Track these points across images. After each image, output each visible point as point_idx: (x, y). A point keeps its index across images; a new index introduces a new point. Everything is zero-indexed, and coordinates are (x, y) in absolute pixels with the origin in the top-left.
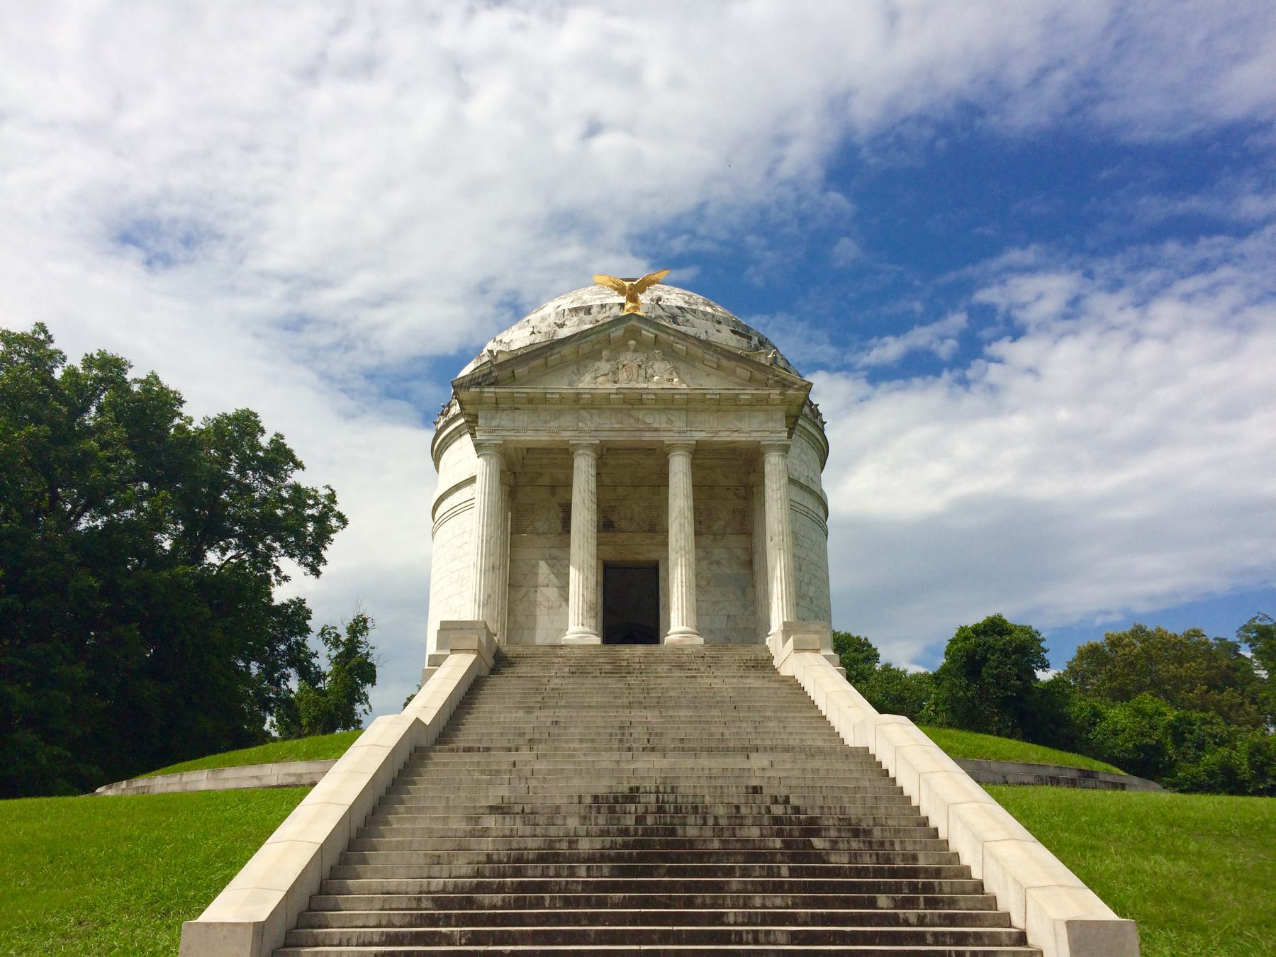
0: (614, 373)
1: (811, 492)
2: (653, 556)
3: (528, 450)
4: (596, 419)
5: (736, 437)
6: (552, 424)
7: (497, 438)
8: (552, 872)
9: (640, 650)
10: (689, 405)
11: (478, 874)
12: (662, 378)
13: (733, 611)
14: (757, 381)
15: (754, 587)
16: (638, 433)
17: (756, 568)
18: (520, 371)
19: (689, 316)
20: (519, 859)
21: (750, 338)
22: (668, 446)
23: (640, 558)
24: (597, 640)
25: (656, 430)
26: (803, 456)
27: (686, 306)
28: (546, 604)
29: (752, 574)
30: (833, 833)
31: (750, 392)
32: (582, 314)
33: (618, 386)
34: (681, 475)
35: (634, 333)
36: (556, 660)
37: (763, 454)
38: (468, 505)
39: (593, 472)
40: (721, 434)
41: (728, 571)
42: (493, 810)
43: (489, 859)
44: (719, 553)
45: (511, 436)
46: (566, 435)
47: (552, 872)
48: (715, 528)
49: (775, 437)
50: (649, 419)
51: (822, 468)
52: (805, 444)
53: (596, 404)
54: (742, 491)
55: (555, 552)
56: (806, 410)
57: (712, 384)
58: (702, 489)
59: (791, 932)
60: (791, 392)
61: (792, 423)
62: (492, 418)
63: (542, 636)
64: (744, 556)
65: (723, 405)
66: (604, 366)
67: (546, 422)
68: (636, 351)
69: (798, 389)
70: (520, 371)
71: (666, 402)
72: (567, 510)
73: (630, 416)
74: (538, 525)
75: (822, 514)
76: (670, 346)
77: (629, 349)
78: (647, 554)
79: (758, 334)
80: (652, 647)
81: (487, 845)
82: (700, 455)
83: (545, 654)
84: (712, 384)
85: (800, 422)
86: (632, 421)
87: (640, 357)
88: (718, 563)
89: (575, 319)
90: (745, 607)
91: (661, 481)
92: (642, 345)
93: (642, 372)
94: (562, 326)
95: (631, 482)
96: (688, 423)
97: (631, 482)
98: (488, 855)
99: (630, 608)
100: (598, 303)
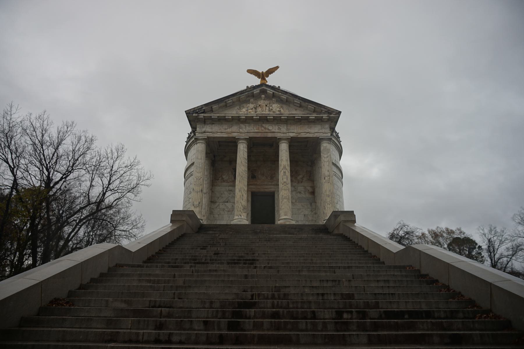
0: (255, 108)
4: (248, 128)
5: (308, 135)
6: (228, 130)
7: (205, 136)
8: (320, 327)
9: (266, 226)
13: (307, 212)
15: (316, 202)
16: (266, 134)
17: (316, 194)
18: (214, 107)
22: (279, 139)
28: (227, 209)
31: (313, 116)
34: (284, 151)
35: (264, 92)
41: (304, 196)
44: (300, 188)
45: (211, 135)
46: (234, 135)
47: (320, 327)
53: (248, 120)
60: (332, 115)
62: (203, 127)
64: (310, 190)
66: (251, 106)
67: (226, 129)
68: (264, 100)
70: (214, 107)
71: (277, 120)
73: (262, 126)
74: (224, 177)
77: (262, 99)
78: (271, 189)
80: (272, 225)
82: (293, 143)
86: (263, 128)
87: (267, 102)
88: (300, 193)
93: (268, 108)
95: (263, 152)
96: (287, 129)
97: (263, 152)
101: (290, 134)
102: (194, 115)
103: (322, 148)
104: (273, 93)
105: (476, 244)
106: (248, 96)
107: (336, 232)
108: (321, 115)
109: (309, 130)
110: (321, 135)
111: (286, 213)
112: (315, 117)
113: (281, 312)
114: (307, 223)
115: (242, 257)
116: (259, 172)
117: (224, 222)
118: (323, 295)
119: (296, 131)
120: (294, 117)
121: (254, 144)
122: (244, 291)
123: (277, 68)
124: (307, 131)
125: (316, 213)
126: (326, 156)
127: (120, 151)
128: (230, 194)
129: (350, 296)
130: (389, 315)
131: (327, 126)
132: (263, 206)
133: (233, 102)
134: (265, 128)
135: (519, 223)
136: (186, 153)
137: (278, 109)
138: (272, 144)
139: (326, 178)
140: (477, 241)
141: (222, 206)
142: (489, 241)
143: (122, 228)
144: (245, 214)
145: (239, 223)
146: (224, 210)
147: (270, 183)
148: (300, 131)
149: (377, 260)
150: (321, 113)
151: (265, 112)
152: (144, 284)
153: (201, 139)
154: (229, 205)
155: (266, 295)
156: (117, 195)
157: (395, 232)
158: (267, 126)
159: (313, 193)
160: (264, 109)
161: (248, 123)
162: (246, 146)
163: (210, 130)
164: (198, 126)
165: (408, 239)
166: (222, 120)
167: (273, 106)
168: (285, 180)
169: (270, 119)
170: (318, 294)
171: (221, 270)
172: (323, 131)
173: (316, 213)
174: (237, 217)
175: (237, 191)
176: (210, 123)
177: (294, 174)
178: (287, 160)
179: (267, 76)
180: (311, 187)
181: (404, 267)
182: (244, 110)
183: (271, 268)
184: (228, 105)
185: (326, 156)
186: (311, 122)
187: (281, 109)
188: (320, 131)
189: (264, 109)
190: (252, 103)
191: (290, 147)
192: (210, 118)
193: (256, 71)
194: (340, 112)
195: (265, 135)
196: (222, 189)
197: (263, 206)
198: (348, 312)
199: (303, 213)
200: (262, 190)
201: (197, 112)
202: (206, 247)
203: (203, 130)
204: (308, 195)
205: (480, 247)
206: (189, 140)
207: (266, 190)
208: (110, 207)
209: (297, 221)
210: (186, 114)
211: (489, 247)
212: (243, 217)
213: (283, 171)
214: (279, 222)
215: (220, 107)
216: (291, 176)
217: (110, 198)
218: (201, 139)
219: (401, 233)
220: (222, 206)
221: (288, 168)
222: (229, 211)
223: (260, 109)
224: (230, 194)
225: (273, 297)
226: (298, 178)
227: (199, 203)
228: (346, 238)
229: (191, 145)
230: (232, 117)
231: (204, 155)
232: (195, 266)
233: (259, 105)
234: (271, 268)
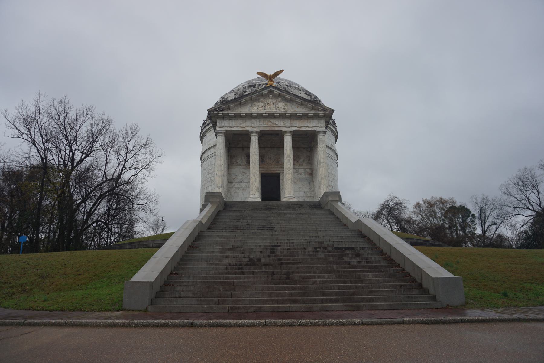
1: (333, 150)
4: (258, 123)
7: (224, 130)
10: (294, 117)
11: (227, 269)
12: (281, 107)
13: (306, 190)
17: (314, 175)
20: (241, 265)
24: (260, 200)
25: (280, 127)
29: (313, 177)
30: (350, 256)
31: (311, 114)
34: (288, 143)
35: (271, 92)
38: (214, 155)
39: (258, 142)
42: (229, 249)
43: (230, 264)
44: (301, 170)
45: (229, 129)
49: (321, 129)
50: (277, 123)
53: (259, 116)
55: (244, 171)
56: (331, 121)
57: (300, 110)
58: (295, 148)
61: (327, 123)
62: (222, 123)
65: (305, 117)
66: (261, 104)
68: (272, 99)
71: (283, 116)
72: (248, 156)
73: (270, 122)
74: (238, 161)
76: (284, 96)
78: (276, 170)
79: (314, 95)
80: (279, 202)
81: (226, 261)
82: (297, 136)
84: (300, 110)
85: (329, 125)
87: (274, 101)
88: (301, 174)
90: (310, 189)
91: (281, 146)
93: (274, 106)
94: (246, 92)
95: (271, 142)
96: (291, 124)
97: (271, 142)
103: (319, 140)
105: (470, 212)
106: (258, 96)
107: (326, 208)
109: (309, 125)
111: (290, 191)
114: (307, 200)
117: (238, 200)
119: (297, 125)
121: (263, 136)
123: (283, 71)
124: (306, 125)
125: (313, 191)
126: (321, 146)
127: (134, 131)
129: (322, 243)
130: (336, 248)
131: (323, 121)
132: (271, 185)
133: (246, 101)
134: (273, 123)
135: (505, 193)
136: (202, 138)
137: (283, 107)
138: (279, 136)
140: (471, 210)
141: (237, 186)
142: (481, 209)
143: (139, 202)
145: (254, 200)
146: (239, 189)
149: (345, 226)
150: (318, 110)
153: (221, 133)
154: (243, 185)
156: (133, 172)
157: (386, 204)
158: (274, 121)
159: (311, 174)
163: (228, 125)
164: (218, 121)
165: (398, 209)
166: (237, 117)
167: (279, 104)
168: (289, 166)
172: (320, 125)
173: (313, 191)
174: (252, 196)
175: (251, 175)
176: (228, 119)
177: (296, 158)
178: (290, 150)
180: (310, 169)
181: (355, 230)
182: (255, 108)
183: (284, 231)
185: (321, 146)
187: (286, 107)
188: (317, 125)
191: (293, 141)
194: (334, 110)
195: (273, 129)
196: (237, 171)
197: (271, 185)
200: (270, 172)
203: (222, 125)
204: (307, 176)
205: (473, 215)
206: (205, 127)
207: (273, 172)
208: (128, 183)
209: (299, 197)
211: (480, 215)
214: (285, 200)
216: (294, 160)
217: (126, 176)
218: (221, 133)
219: (391, 204)
220: (237, 186)
221: (291, 156)
225: (287, 243)
226: (300, 162)
228: (331, 213)
229: (206, 131)
231: (223, 146)
234: (284, 231)
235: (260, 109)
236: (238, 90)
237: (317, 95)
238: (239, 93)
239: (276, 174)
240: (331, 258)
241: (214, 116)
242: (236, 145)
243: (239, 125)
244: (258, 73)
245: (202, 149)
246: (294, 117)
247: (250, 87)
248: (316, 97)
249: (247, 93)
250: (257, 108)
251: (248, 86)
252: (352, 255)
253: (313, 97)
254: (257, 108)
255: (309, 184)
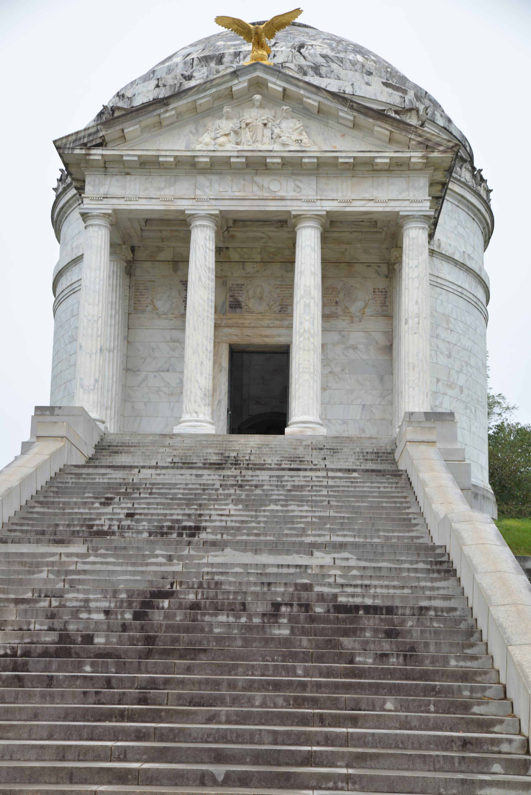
1: (469, 270)
2: (282, 340)
3: (147, 221)
4: (216, 187)
5: (371, 207)
7: (107, 207)
10: (325, 168)
14: (398, 142)
19: (334, 66)
21: (405, 92)
23: (270, 341)
25: (282, 199)
26: (460, 229)
27: (331, 54)
28: (166, 390)
31: (385, 156)
32: (213, 64)
33: (240, 148)
35: (259, 85)
36: (162, 450)
37: (402, 227)
40: (355, 203)
41: (365, 357)
48: (353, 309)
49: (416, 207)
51: (486, 242)
52: (463, 215)
54: (384, 269)
59: (58, 747)
60: (436, 154)
63: (154, 426)
65: (361, 168)
66: (226, 125)
67: (160, 189)
68: (261, 106)
69: (444, 152)
71: (292, 166)
73: (253, 182)
74: (159, 304)
75: (480, 294)
77: (253, 105)
78: (273, 337)
79: (416, 86)
82: (332, 227)
83: (153, 443)
84: (347, 146)
86: (255, 188)
87: (266, 114)
88: (355, 348)
89: (205, 69)
90: (382, 396)
92: (270, 100)
94: (189, 78)
95: (255, 248)
97: (255, 248)
98: (13, 648)
99: (257, 394)
100: (232, 51)
101: (325, 203)
102: (77, 151)
104: (285, 89)
106: (217, 97)
108: (407, 155)
110: (403, 208)
112: (391, 158)
113: (203, 603)
115: (178, 521)
116: (251, 293)
118: (269, 584)
119: (339, 196)
120: (337, 158)
121: (230, 228)
122: (163, 578)
124: (368, 196)
128: (173, 349)
136: (57, 222)
137: (295, 136)
139: (410, 321)
144: (208, 410)
146: (158, 391)
147: (278, 323)
148: (350, 195)
151: (263, 144)
152: (17, 568)
155: (191, 584)
160: (260, 134)
161: (217, 174)
162: (213, 235)
163: (119, 192)
164: (88, 180)
166: (149, 166)
167: (284, 124)
168: (307, 325)
169: (273, 163)
170: (263, 583)
171: (132, 547)
176: (120, 173)
179: (271, 36)
182: (207, 138)
184: (164, 123)
186: (381, 170)
187: (304, 137)
189: (260, 134)
190: (228, 118)
191: (325, 239)
192: (119, 160)
193: (239, 21)
196: (153, 333)
198: (286, 605)
199: (359, 401)
201: (85, 144)
202: (112, 499)
203: (103, 191)
210: (58, 148)
212: (201, 417)
213: (302, 304)
215: (143, 130)
222: (171, 395)
223: (249, 135)
224: (173, 349)
227: (97, 381)
230: (175, 157)
232: (92, 541)
233: (247, 125)
235: (222, 140)
236: (170, 70)
237: (426, 88)
238: (170, 81)
239: (281, 346)
240: (305, 641)
241: (80, 159)
242: (146, 254)
243: (153, 193)
244: (221, 20)
245: (57, 259)
246: (325, 168)
247: (205, 60)
248: (422, 95)
249: (192, 83)
250: (212, 139)
251: (200, 60)
252: (376, 631)
253: (411, 95)
254: (212, 139)
255: (381, 379)
